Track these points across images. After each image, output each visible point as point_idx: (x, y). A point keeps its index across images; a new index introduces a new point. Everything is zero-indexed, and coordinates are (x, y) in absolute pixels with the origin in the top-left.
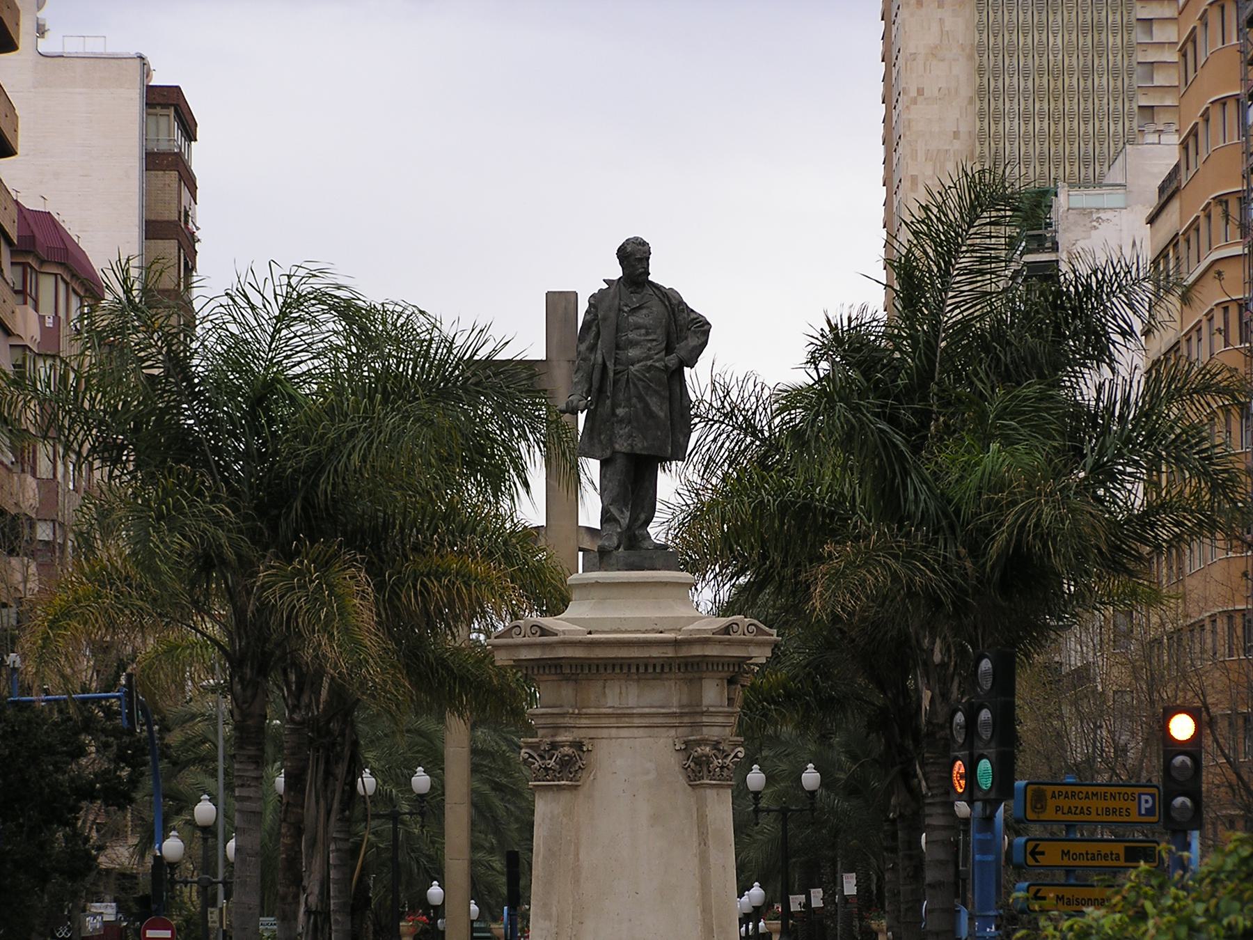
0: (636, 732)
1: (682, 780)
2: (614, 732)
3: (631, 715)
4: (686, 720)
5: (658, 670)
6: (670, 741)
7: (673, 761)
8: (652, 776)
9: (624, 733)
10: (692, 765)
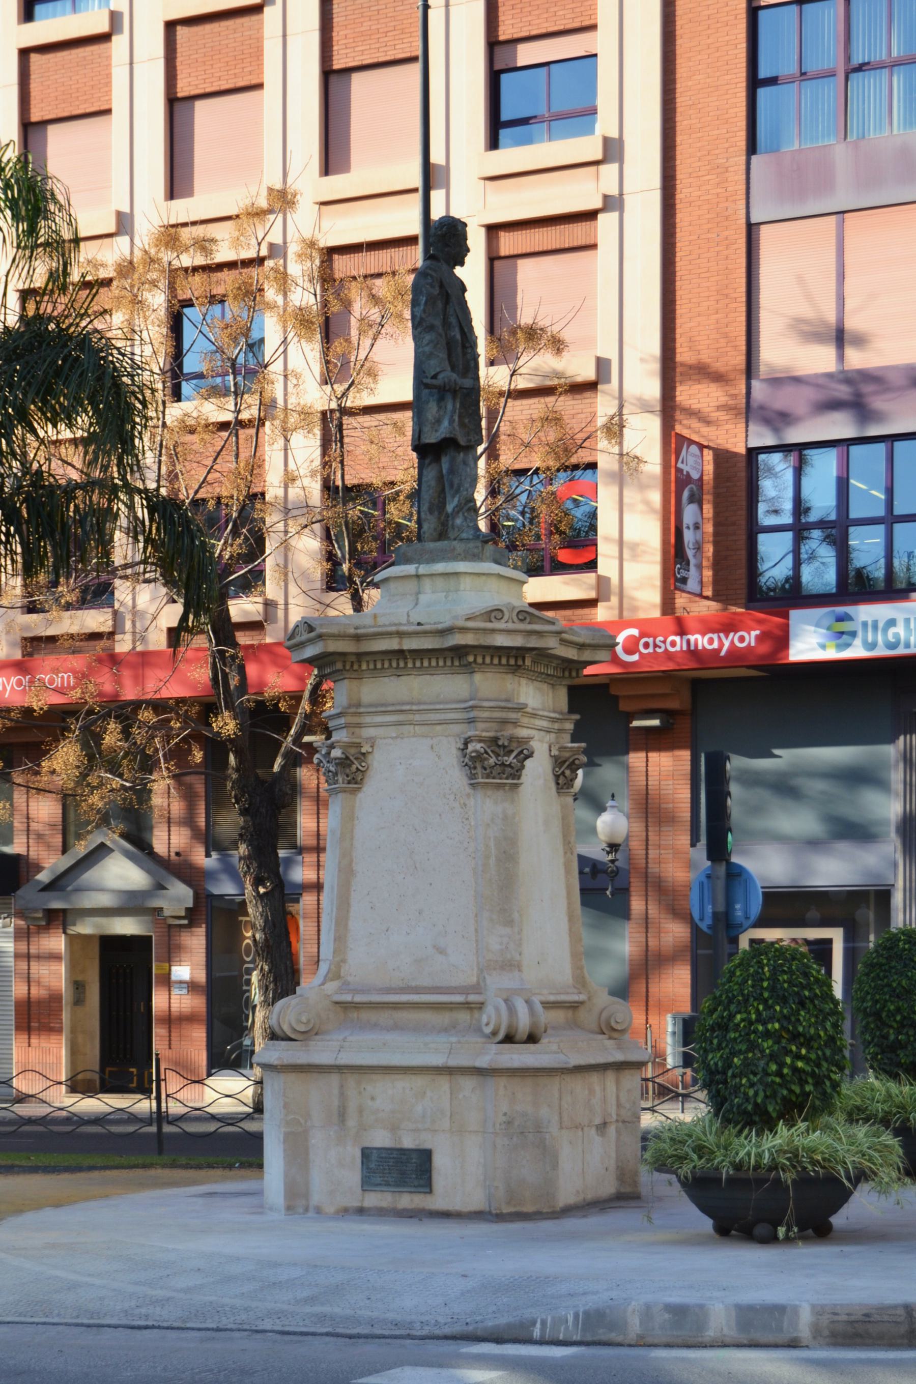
4: (556, 726)
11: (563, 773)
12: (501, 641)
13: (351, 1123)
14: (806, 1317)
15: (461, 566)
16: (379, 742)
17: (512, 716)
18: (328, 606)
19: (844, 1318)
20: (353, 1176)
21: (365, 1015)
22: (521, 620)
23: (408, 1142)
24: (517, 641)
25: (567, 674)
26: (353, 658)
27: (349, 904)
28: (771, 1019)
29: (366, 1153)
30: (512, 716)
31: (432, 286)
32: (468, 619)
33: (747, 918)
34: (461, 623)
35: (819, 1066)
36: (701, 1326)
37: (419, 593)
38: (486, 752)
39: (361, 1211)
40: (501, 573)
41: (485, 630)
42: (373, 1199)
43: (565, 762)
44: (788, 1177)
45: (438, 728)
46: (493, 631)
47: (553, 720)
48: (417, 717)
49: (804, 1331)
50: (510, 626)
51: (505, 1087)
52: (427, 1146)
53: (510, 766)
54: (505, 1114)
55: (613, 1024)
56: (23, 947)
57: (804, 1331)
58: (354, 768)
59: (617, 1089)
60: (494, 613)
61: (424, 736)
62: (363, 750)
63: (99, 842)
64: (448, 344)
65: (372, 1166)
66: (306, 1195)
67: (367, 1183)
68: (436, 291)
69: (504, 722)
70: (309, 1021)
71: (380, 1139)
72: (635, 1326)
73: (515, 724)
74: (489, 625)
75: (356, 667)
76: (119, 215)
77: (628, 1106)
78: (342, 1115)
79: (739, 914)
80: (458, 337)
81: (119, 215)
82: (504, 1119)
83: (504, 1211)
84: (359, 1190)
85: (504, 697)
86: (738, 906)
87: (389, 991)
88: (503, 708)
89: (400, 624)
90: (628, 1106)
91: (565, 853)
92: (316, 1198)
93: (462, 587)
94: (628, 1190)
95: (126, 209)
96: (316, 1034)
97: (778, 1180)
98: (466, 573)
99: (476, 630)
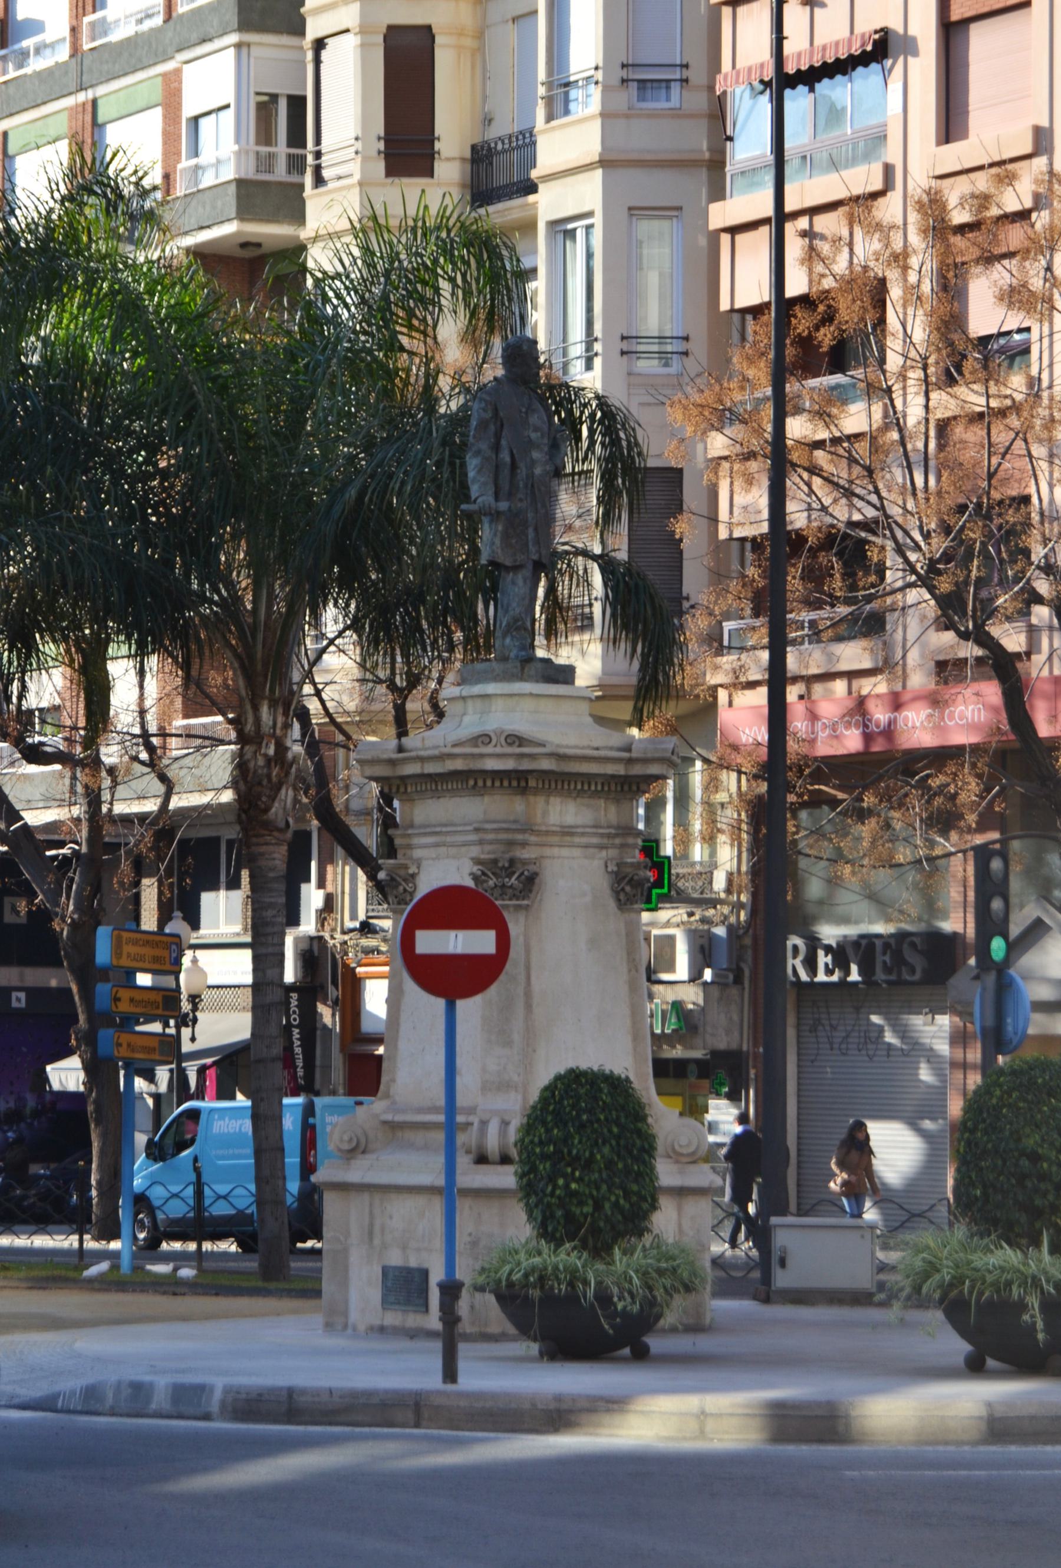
0: (577, 852)
1: (612, 904)
2: (556, 851)
3: (572, 834)
4: (617, 841)
5: (599, 788)
6: (602, 862)
7: (603, 883)
8: (588, 899)
9: (565, 852)
10: (628, 889)
11: (623, 889)
12: (491, 765)
13: (377, 1241)
14: (218, 1395)
15: (491, 688)
16: (424, 863)
17: (519, 837)
18: (734, 685)
19: (244, 1396)
20: (375, 1294)
21: (409, 1135)
22: (510, 744)
23: (413, 1263)
24: (509, 765)
25: (626, 788)
26: (398, 782)
27: (398, 1024)
28: (550, 1141)
29: (385, 1271)
30: (519, 837)
31: (484, 410)
32: (454, 746)
33: (1016, 1033)
34: (448, 750)
35: (598, 1188)
36: (148, 1400)
37: (464, 714)
38: (484, 874)
39: (382, 1330)
40: (534, 692)
41: (473, 756)
42: (392, 1318)
43: (624, 878)
44: (535, 1293)
45: (463, 849)
46: (482, 756)
47: (609, 836)
48: (449, 839)
49: (215, 1407)
50: (498, 750)
51: (471, 1208)
52: (425, 1265)
53: (511, 887)
54: (470, 1235)
55: (677, 1147)
56: (959, 1054)
57: (215, 1407)
58: (401, 888)
59: (679, 1214)
60: (484, 738)
61: (454, 857)
62: (411, 871)
63: (1034, 916)
64: (497, 466)
65: (389, 1284)
66: (345, 1314)
67: (386, 1303)
68: (489, 415)
69: (511, 843)
70: (351, 1140)
71: (395, 1259)
72: (110, 1400)
73: (524, 844)
74: (476, 751)
75: (402, 790)
76: (1038, 131)
77: (691, 1233)
78: (371, 1233)
79: (1010, 1028)
80: (508, 459)
81: (1038, 131)
82: (468, 1239)
83: (468, 1331)
84: (379, 1307)
85: (512, 818)
86: (1009, 1020)
87: (420, 1110)
88: (507, 830)
89: (438, 747)
90: (691, 1233)
91: (630, 971)
92: (354, 1316)
93: (493, 708)
94: (691, 1321)
95: (1045, 123)
96: (364, 1152)
97: (526, 1297)
98: (496, 695)
99: (465, 756)
